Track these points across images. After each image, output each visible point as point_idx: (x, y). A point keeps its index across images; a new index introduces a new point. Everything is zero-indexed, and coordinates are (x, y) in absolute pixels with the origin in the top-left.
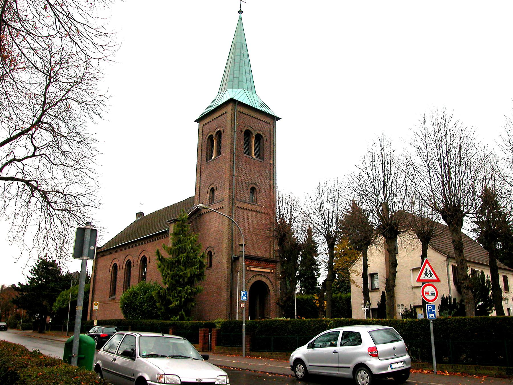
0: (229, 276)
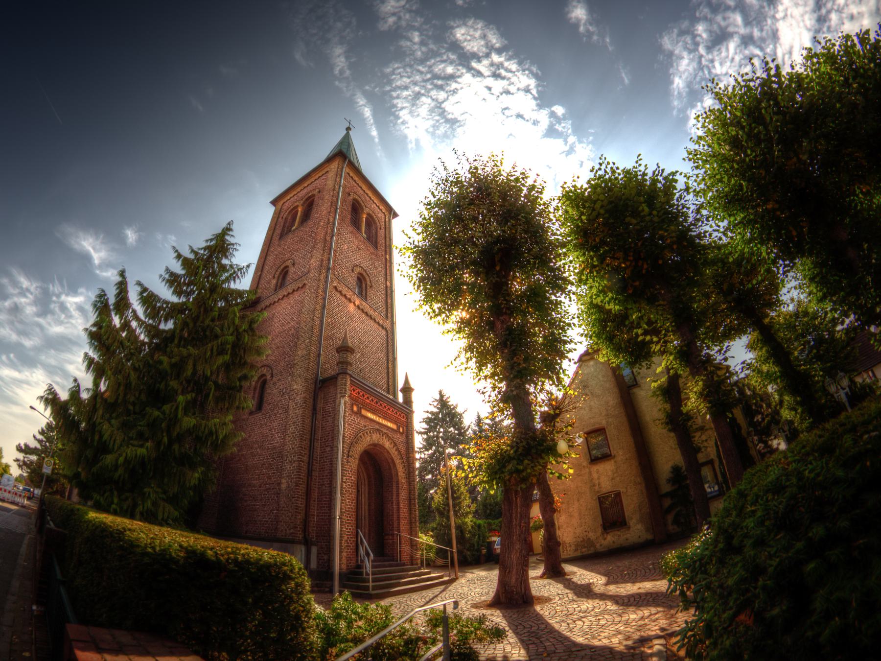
0: (308, 421)
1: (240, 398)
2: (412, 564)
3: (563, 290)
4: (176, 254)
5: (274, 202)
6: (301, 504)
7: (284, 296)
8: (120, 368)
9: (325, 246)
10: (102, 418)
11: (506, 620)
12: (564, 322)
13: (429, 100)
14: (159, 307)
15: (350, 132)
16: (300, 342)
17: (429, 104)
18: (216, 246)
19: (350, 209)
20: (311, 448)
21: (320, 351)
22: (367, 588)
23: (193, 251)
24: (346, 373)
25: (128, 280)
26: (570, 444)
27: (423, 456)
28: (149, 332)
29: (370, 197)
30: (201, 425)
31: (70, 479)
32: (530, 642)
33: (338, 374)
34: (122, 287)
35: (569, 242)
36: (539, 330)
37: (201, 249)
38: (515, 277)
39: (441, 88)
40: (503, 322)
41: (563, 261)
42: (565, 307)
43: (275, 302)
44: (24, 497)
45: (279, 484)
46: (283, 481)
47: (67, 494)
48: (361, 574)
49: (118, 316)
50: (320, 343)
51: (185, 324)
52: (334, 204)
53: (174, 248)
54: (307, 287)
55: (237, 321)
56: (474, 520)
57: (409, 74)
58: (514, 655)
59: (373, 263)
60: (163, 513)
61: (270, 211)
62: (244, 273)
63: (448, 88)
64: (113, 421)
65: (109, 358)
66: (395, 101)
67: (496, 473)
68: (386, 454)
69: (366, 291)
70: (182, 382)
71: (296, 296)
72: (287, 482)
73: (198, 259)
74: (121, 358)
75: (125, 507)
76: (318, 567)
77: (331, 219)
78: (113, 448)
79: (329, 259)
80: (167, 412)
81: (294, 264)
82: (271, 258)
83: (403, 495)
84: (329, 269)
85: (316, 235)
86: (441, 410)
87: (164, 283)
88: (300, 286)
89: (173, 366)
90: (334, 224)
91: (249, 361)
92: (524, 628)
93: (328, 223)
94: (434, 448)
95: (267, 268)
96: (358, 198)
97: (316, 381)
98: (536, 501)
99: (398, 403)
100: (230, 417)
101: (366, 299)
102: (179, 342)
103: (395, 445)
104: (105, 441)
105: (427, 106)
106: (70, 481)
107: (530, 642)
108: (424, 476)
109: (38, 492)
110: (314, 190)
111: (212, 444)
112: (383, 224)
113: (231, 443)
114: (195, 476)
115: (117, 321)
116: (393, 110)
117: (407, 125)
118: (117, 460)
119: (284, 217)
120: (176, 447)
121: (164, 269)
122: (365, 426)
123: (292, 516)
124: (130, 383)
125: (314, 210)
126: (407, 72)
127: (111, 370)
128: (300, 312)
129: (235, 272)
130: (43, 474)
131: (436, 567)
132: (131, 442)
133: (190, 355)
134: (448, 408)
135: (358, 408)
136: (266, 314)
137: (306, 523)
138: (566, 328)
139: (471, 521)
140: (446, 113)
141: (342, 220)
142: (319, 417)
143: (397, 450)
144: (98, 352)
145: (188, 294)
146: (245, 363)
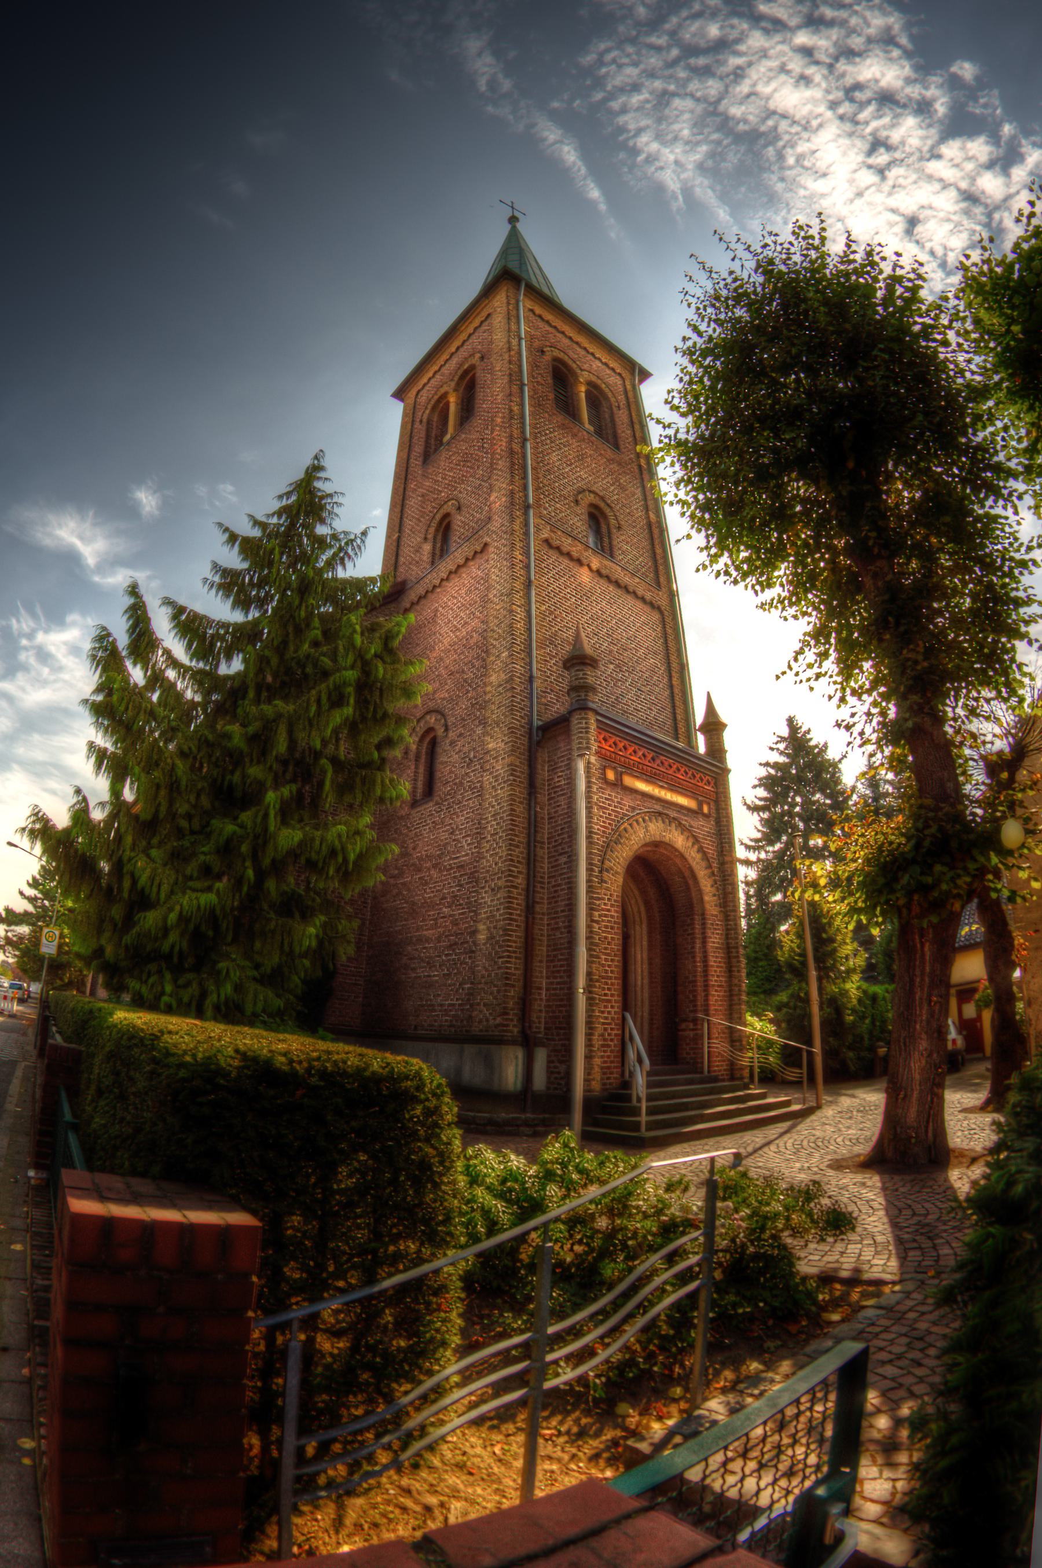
0: (520, 809)
1: (383, 782)
2: (732, 1078)
3: (995, 492)
4: (227, 535)
5: (399, 394)
6: (516, 968)
7: (451, 572)
8: (155, 757)
9: (513, 464)
10: (133, 849)
11: (885, 1196)
12: (1012, 559)
13: (689, 103)
14: (213, 636)
15: (519, 226)
16: (492, 658)
17: (692, 111)
18: (299, 504)
19: (550, 381)
20: (531, 861)
21: (531, 670)
22: (636, 1126)
23: (256, 523)
24: (586, 709)
25: (145, 599)
26: (1031, 827)
27: (763, 855)
28: (200, 683)
29: (585, 349)
30: (313, 839)
31: (88, 961)
32: (915, 1245)
33: (571, 712)
34: (138, 615)
35: (998, 384)
36: (961, 581)
37: (273, 515)
38: (889, 477)
39: (706, 72)
40: (875, 576)
41: (991, 429)
42: (1010, 526)
43: (435, 587)
44: (12, 999)
45: (474, 933)
46: (481, 927)
47: (89, 985)
48: (628, 1098)
49: (139, 666)
50: (530, 654)
51: (262, 661)
52: (515, 377)
53: (220, 525)
54: (491, 549)
55: (358, 639)
56: (865, 985)
57: (634, 57)
58: (875, 1269)
59: (617, 480)
60: (255, 1004)
61: (396, 411)
62: (359, 547)
63: (723, 70)
64: (154, 852)
65: (134, 744)
66: (621, 120)
67: (880, 892)
68: (678, 861)
69: (610, 538)
70: (271, 768)
71: (474, 570)
72: (488, 929)
73: (269, 536)
74: (155, 740)
75: (186, 999)
76: (548, 1088)
77: (516, 408)
78: (158, 900)
79: (525, 488)
80: (249, 824)
81: (459, 508)
82: (413, 502)
83: (715, 940)
84: (527, 507)
85: (492, 445)
86: (794, 757)
87: (214, 591)
88: (479, 548)
89: (252, 739)
90: (522, 417)
91: (391, 711)
92: (914, 1214)
93: (512, 418)
94: (784, 838)
95: (408, 523)
96: (561, 355)
97: (531, 729)
98: (969, 947)
99: (698, 757)
100: (367, 819)
101: (612, 555)
102: (258, 694)
103: (696, 840)
104: (143, 889)
105: (687, 116)
106: (88, 965)
107: (915, 1245)
108: (767, 896)
109: (35, 988)
110: (472, 355)
111: (338, 870)
112: (621, 397)
113: (374, 866)
114: (310, 932)
115: (137, 675)
116: (621, 138)
117: (658, 164)
118: (165, 919)
119: (425, 420)
120: (271, 884)
121: (209, 566)
122: (634, 809)
123: (499, 992)
124: (177, 782)
125: (480, 395)
126: (628, 55)
127: (139, 764)
128: (485, 601)
129: (341, 549)
130: (44, 957)
131: (786, 1084)
132: (190, 884)
133: (279, 716)
134: (808, 754)
135: (616, 773)
136: (412, 617)
137: (525, 1004)
138: (1016, 572)
139: (858, 988)
140: (731, 123)
141: (538, 404)
142: (543, 798)
143: (701, 850)
144: (112, 736)
145: (261, 603)
146: (385, 715)
